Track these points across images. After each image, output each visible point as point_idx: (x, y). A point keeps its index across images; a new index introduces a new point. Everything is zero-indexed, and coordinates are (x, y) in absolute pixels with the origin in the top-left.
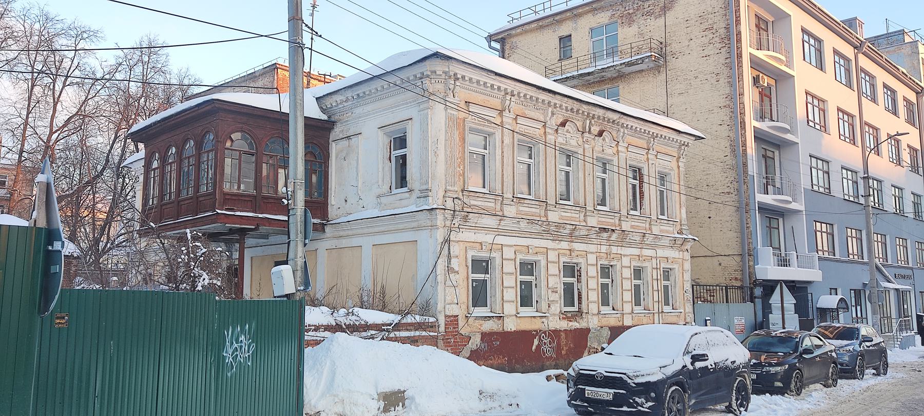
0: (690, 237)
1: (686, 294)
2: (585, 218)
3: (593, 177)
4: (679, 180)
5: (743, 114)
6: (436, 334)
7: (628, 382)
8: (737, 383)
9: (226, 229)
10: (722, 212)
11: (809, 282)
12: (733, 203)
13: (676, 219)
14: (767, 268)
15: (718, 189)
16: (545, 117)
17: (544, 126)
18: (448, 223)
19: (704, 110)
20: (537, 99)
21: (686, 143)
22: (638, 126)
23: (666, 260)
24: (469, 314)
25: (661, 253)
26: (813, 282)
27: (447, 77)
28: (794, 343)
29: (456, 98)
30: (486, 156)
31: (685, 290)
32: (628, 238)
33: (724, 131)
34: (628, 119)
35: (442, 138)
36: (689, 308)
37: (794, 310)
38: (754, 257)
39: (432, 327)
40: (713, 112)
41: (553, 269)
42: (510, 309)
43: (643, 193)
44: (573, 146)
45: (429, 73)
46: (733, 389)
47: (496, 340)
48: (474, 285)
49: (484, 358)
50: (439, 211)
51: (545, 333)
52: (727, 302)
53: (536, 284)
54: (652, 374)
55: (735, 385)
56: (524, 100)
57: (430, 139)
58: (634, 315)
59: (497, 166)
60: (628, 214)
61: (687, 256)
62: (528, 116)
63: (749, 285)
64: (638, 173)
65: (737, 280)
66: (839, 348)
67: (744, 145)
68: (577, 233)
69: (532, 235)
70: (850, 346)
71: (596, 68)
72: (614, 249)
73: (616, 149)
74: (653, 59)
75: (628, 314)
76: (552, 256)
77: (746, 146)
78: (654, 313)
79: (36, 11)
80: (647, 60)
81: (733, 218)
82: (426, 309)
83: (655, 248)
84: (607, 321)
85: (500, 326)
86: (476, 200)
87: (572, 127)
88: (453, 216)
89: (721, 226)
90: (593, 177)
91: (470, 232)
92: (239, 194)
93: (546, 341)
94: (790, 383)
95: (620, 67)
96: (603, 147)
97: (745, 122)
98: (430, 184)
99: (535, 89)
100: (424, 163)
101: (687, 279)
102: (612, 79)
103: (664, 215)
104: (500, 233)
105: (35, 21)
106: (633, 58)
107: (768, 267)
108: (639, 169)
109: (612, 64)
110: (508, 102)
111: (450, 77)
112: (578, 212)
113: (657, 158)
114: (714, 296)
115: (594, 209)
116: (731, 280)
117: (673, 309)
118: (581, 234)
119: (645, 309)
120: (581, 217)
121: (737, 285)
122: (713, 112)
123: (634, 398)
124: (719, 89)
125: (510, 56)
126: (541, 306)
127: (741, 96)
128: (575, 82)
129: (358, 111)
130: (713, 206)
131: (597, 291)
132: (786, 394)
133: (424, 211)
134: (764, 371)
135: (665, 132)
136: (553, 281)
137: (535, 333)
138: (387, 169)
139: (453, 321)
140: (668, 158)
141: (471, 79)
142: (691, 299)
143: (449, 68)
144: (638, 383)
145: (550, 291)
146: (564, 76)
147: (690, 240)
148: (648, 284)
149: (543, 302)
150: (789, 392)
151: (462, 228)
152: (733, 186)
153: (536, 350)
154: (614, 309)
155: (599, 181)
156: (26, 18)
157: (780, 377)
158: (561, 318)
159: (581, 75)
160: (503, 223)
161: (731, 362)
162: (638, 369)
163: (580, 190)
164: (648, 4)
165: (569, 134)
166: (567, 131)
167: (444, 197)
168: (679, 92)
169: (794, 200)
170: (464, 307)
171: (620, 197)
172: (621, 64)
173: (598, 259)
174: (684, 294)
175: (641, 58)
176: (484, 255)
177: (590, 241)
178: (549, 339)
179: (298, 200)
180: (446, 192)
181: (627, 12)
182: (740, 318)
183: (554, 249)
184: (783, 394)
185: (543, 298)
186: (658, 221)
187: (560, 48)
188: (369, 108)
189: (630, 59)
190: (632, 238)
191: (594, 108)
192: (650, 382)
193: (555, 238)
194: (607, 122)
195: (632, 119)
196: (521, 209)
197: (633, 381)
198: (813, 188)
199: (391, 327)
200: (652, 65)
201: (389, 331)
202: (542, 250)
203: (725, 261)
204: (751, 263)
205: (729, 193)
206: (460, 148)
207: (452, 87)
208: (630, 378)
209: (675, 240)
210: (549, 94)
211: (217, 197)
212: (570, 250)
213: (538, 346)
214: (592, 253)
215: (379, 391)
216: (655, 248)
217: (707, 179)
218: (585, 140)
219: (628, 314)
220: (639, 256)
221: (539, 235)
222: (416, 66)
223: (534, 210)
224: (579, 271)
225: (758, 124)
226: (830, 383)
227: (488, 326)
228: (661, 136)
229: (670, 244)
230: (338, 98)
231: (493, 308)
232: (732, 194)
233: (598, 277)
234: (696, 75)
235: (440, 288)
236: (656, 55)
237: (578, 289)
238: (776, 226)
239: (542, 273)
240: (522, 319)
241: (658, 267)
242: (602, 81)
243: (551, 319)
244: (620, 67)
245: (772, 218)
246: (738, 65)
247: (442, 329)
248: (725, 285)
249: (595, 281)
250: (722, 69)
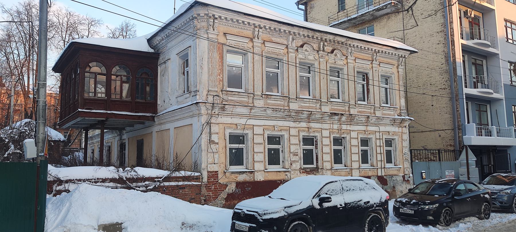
0: (408, 117)
2: (320, 107)
3: (327, 80)
4: (399, 80)
5: (452, 35)
6: (200, 183)
7: (258, 218)
8: (370, 218)
9: (96, 121)
10: (440, 101)
11: (509, 147)
12: (448, 95)
13: (396, 106)
14: (471, 137)
15: (438, 87)
16: (288, 42)
17: (287, 47)
18: (209, 112)
19: (427, 35)
20: (280, 30)
21: (403, 56)
22: (363, 46)
23: (388, 133)
24: (226, 170)
25: (382, 129)
26: (512, 146)
27: (208, 18)
28: (449, 188)
29: (215, 31)
30: (310, 78)
31: (404, 153)
32: (356, 119)
33: (441, 48)
34: (353, 41)
35: (206, 57)
36: (407, 165)
37: (466, 165)
38: (462, 130)
39: (197, 179)
40: (433, 36)
41: (294, 140)
43: (369, 90)
44: (311, 60)
45: (196, 16)
46: (365, 222)
47: (248, 187)
48: (305, 152)
49: (239, 199)
50: (202, 104)
52: (440, 160)
53: (282, 150)
54: (276, 213)
55: (368, 219)
56: (270, 31)
57: (198, 58)
58: (360, 170)
59: (249, 75)
60: (355, 104)
61: (406, 130)
62: (274, 41)
63: (459, 149)
64: (365, 77)
65: (451, 146)
66: (500, 191)
67: (454, 56)
68: (313, 117)
69: (277, 118)
70: (508, 189)
71: (359, 15)
72: (344, 127)
73: (371, 65)
74: (393, 4)
75: (356, 169)
76: (293, 132)
77: (455, 56)
78: (378, 168)
79: (64, 11)
80: (389, 6)
81: (448, 105)
82: (196, 167)
83: (378, 125)
85: (251, 177)
86: (233, 97)
87: (310, 47)
88: (213, 107)
89: (440, 111)
90: (327, 80)
91: (227, 117)
92: (95, 99)
94: (440, 217)
95: (373, 12)
96: (335, 60)
97: (454, 41)
98: (198, 87)
99: (276, 23)
100: (195, 73)
101: (406, 146)
102: (370, 21)
103: (388, 104)
104: (251, 118)
105: (64, 17)
106: (380, 6)
107: (472, 137)
108: (366, 74)
109: (368, 11)
110: (256, 33)
111: (210, 17)
112: (315, 103)
113: (356, 62)
114: (436, 157)
115: (380, 106)
116: (447, 146)
117: (395, 166)
118: (316, 117)
119: (371, 166)
120: (317, 106)
121: (451, 149)
122: (433, 36)
123: (261, 230)
124: (437, 21)
125: (310, 13)
126: (285, 165)
127: (451, 24)
128: (347, 25)
129: (169, 45)
130: (435, 98)
131: (330, 154)
132: (438, 225)
134: (420, 209)
135: (384, 49)
136: (326, 149)
137: (279, 182)
138: (181, 79)
139: (214, 175)
140: (390, 66)
141: (249, 23)
142: (409, 159)
143: (208, 12)
144: (265, 219)
145: (291, 155)
146: (340, 22)
147: (407, 120)
148: (373, 149)
149: (286, 162)
150: (440, 224)
151: (219, 115)
152: (447, 84)
154: (345, 166)
155: (384, 89)
156: (59, 15)
157: (432, 212)
158: (301, 172)
159: (349, 20)
160: (253, 111)
161: (365, 203)
162: (266, 209)
163: (316, 89)
165: (307, 52)
166: (306, 50)
167: (207, 95)
168: (411, 25)
169: (497, 92)
170: (223, 166)
171: (349, 92)
172: (373, 10)
173: (331, 134)
174: (403, 155)
175: (385, 5)
176: (239, 132)
177: (324, 121)
179: (40, 95)
180: (208, 92)
182: (450, 171)
183: (295, 127)
184: (434, 226)
185: (286, 159)
186: (381, 108)
187: (339, 5)
188: (173, 43)
189: (378, 6)
190: (359, 119)
191: (325, 35)
192: (273, 218)
193: (296, 120)
194: (338, 44)
195: (356, 41)
196: (269, 101)
197: (261, 218)
198: (512, 83)
199: (161, 180)
200: (393, 9)
201: (161, 182)
202: (285, 128)
203: (443, 134)
204: (460, 135)
205: (444, 89)
206: (220, 63)
207: (212, 23)
208: (260, 216)
209: (395, 120)
210: (288, 26)
211: (79, 101)
212: (308, 128)
214: (326, 129)
215: (99, 224)
216: (378, 125)
217: (430, 80)
218: (320, 56)
219: (356, 169)
220: (365, 131)
221: (283, 118)
222: (189, 12)
223: (279, 102)
224: (316, 141)
225: (464, 42)
226: (483, 217)
227: (241, 178)
228: (382, 51)
229: (391, 122)
230: (158, 38)
231: (247, 166)
232: (447, 89)
233: (331, 145)
234: (421, 13)
235: (204, 154)
236: (395, 2)
237: (316, 153)
238: (485, 110)
239: (285, 143)
240: (270, 173)
241: (381, 138)
242: (363, 23)
243: (292, 172)
244: (373, 12)
245: (481, 104)
246: (448, 3)
247: (205, 180)
248: (444, 149)
249: (328, 148)
250: (438, 7)
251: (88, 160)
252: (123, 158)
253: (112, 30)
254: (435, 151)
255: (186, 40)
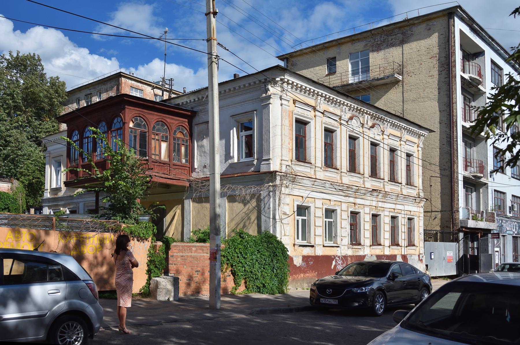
1: (420, 235)
42: (319, 241)
47: (311, 261)
51: (339, 257)
61: (422, 210)
84: (375, 251)
93: (339, 263)
133: (267, 174)
137: (333, 257)
153: (334, 268)
164: (391, 38)
171: (384, 169)
178: (341, 262)
181: (376, 43)
213: (335, 266)
251: (497, 237)
252: (190, 226)
253: (20, 55)
254: (433, 231)
255: (140, 80)
